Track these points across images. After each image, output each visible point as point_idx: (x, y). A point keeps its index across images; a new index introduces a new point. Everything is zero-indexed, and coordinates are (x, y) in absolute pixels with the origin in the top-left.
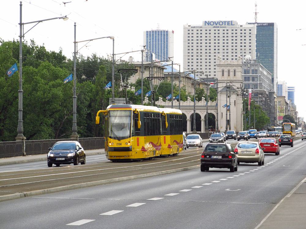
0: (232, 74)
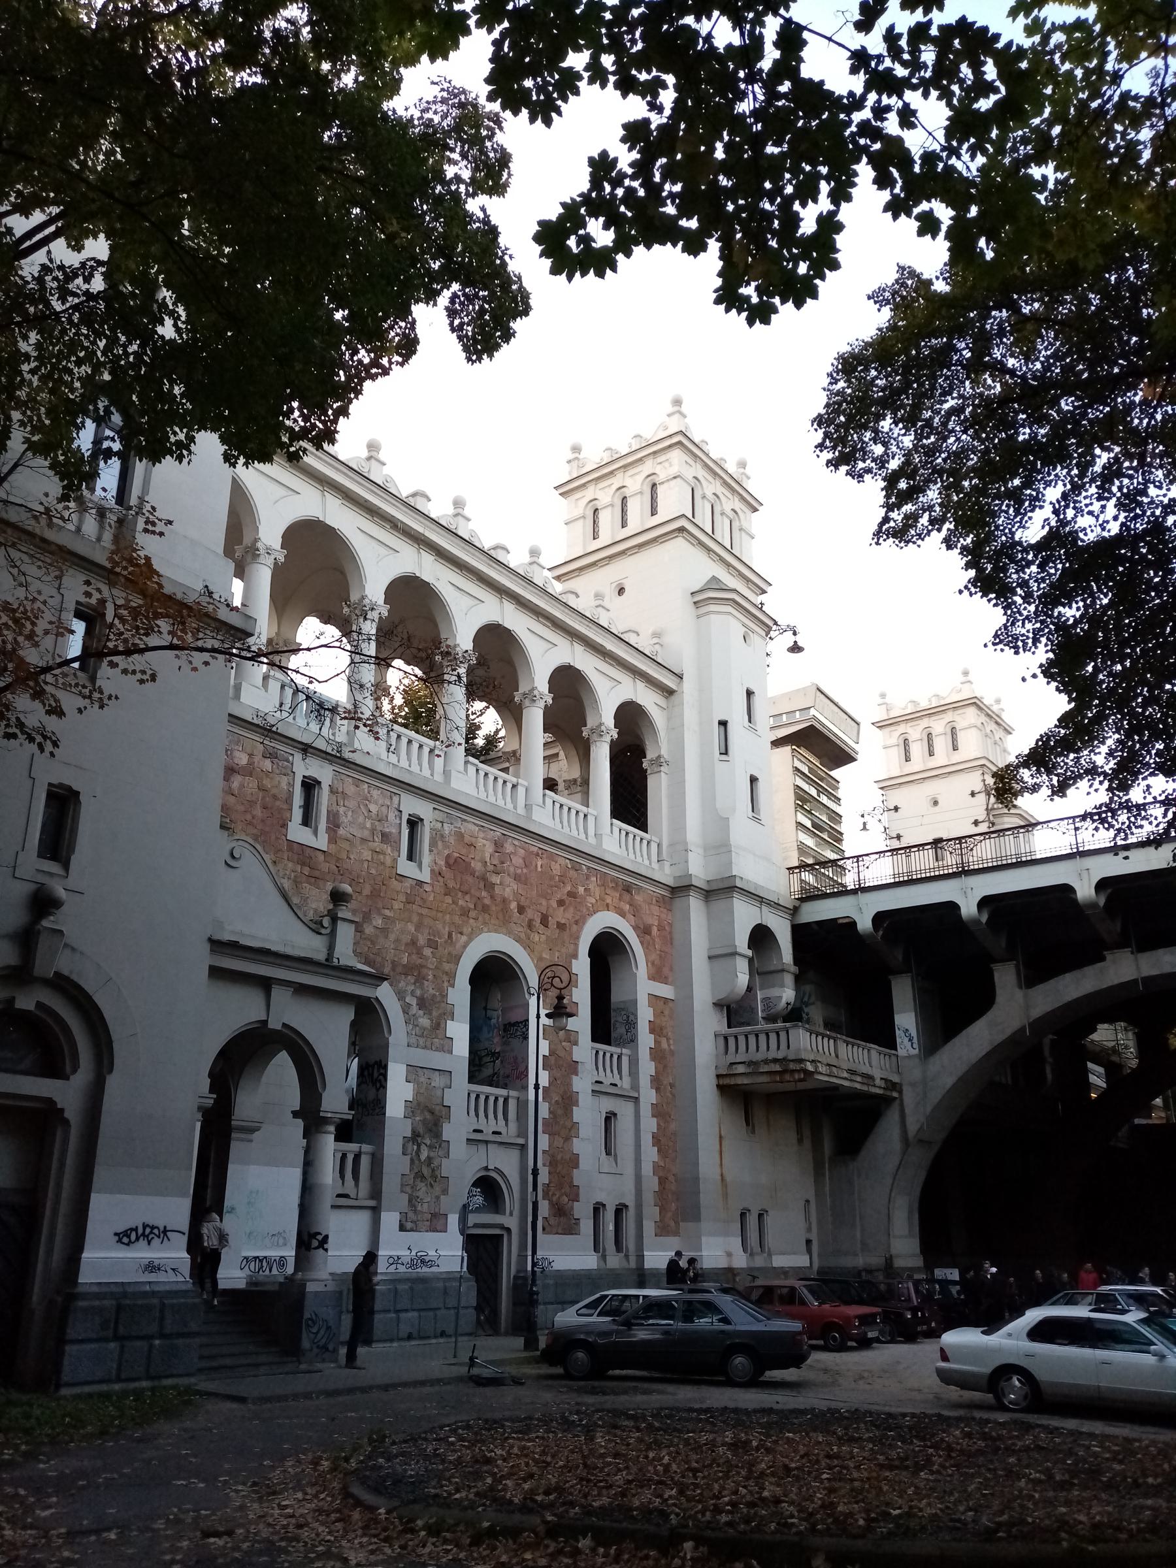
0: (941, 744)
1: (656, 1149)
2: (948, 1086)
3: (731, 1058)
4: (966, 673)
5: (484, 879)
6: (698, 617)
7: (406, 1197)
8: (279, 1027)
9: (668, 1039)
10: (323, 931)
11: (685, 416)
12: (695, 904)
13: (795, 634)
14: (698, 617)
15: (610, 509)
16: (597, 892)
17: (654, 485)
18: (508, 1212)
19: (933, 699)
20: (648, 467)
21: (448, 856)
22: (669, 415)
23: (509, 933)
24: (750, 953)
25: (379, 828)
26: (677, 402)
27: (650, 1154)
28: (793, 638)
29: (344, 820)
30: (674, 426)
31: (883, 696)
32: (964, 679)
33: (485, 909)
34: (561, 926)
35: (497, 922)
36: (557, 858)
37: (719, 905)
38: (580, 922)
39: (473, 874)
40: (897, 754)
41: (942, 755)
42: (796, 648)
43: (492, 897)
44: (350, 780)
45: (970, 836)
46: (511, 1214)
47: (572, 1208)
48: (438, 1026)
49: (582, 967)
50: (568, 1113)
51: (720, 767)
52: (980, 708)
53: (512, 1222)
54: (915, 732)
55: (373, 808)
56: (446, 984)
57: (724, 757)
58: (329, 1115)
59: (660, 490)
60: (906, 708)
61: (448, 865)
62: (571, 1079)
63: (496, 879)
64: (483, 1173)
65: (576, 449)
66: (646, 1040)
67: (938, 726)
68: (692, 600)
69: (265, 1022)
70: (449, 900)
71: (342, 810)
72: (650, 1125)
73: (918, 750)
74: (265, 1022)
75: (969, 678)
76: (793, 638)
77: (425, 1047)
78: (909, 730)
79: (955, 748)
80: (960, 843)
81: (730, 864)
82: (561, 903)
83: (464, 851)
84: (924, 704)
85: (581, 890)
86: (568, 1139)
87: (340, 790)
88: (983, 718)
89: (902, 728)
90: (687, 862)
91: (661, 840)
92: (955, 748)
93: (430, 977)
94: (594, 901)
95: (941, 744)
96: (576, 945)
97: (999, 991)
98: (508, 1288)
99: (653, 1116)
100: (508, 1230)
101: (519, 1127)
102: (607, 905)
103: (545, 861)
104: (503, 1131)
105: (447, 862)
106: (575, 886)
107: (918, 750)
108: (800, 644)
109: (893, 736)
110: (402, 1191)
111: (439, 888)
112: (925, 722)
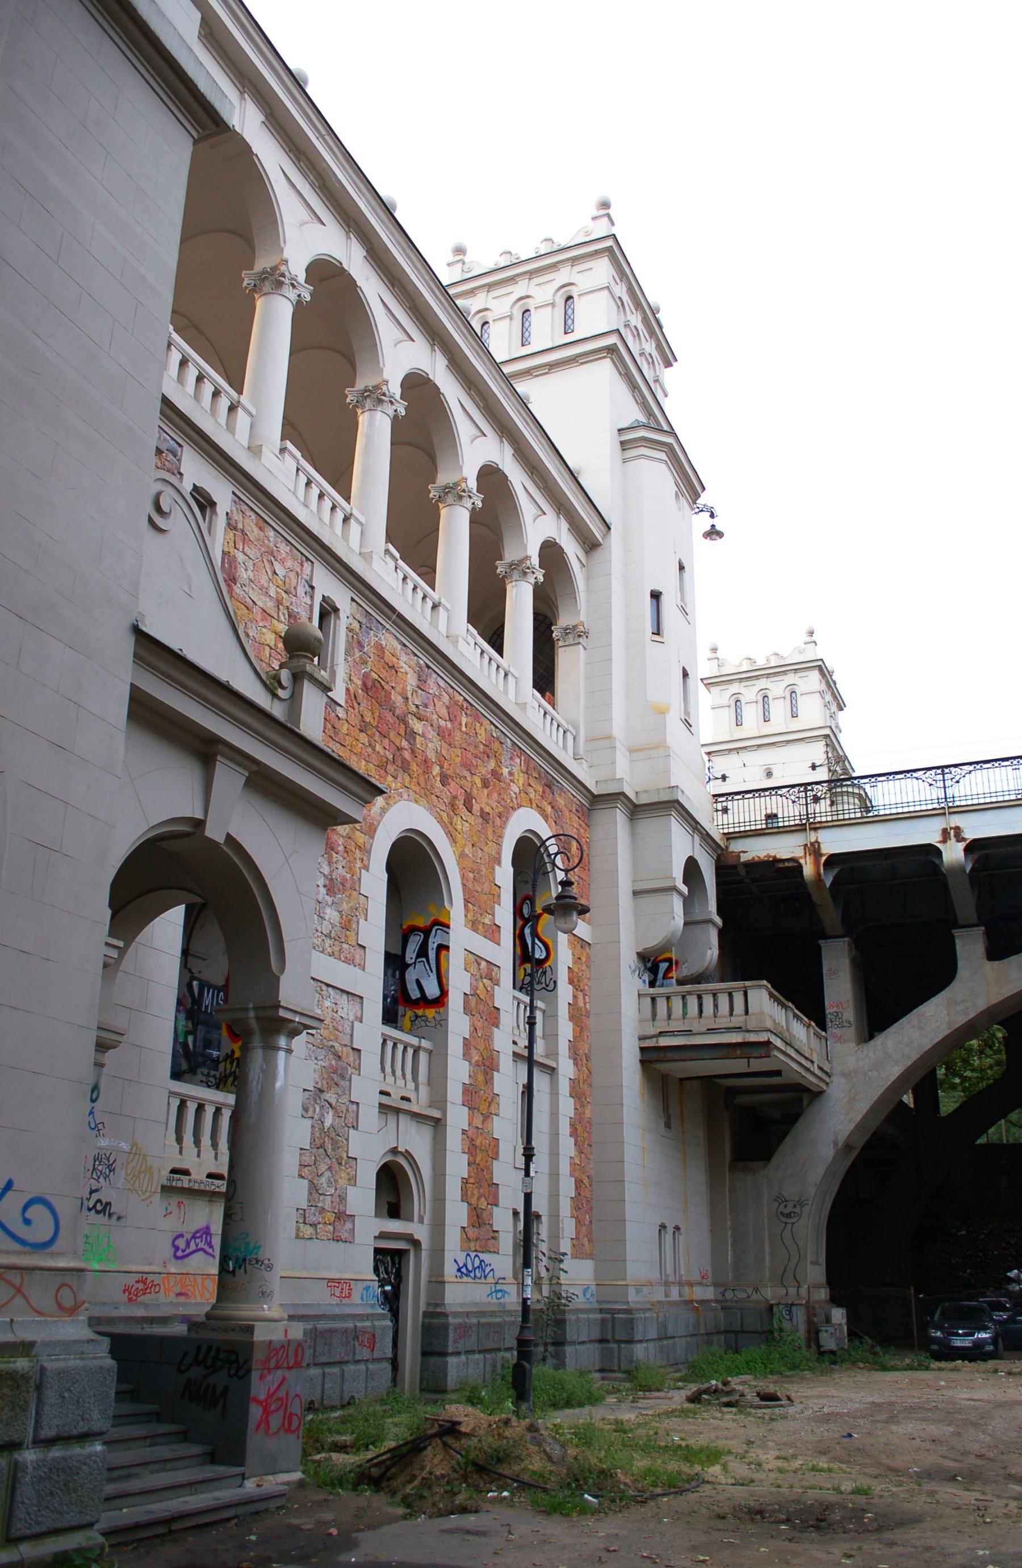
0: (779, 710)
1: (572, 1140)
2: (893, 1078)
3: (662, 1026)
4: (811, 633)
5: (403, 720)
6: (625, 461)
7: (305, 1183)
8: (220, 839)
9: (585, 995)
10: (281, 693)
11: (613, 224)
12: (620, 817)
13: (712, 516)
14: (625, 461)
15: (508, 320)
16: (521, 779)
17: (570, 298)
18: (416, 1218)
19: (772, 658)
20: (564, 275)
21: (366, 676)
22: (594, 219)
23: (431, 808)
24: (685, 889)
25: (286, 603)
26: (605, 205)
27: (567, 1146)
28: (710, 522)
29: (243, 575)
30: (601, 229)
31: (714, 650)
32: (809, 639)
33: (405, 767)
34: (484, 816)
35: (417, 789)
36: (483, 719)
37: (648, 825)
38: (504, 816)
39: (392, 710)
40: (728, 715)
41: (780, 720)
42: (713, 533)
43: (413, 751)
44: (254, 516)
45: (956, 766)
46: (421, 1220)
47: (491, 1214)
48: (348, 924)
49: (505, 875)
50: (489, 1081)
51: (653, 650)
52: (823, 675)
53: (420, 1231)
54: (749, 693)
55: (280, 571)
56: (359, 864)
57: (656, 638)
58: (288, 1015)
59: (578, 304)
60: (741, 665)
61: (365, 687)
62: (492, 1033)
63: (418, 726)
64: (389, 1158)
65: (460, 250)
66: (565, 992)
67: (777, 688)
68: (617, 440)
69: (199, 824)
70: (363, 738)
71: (240, 557)
72: (567, 1107)
73: (751, 714)
74: (199, 824)
75: (815, 637)
76: (710, 522)
77: (332, 955)
78: (742, 690)
79: (794, 715)
80: (943, 774)
81: (667, 772)
82: (485, 784)
83: (384, 674)
84: (761, 662)
85: (505, 771)
86: (487, 1117)
87: (240, 526)
88: (824, 687)
89: (735, 688)
90: (614, 763)
91: (577, 731)
92: (794, 715)
93: (341, 848)
94: (517, 790)
95: (779, 710)
96: (499, 845)
97: (960, 964)
98: (413, 1334)
99: (571, 1096)
100: (416, 1243)
101: (432, 1094)
102: (530, 800)
103: (470, 719)
104: (412, 1096)
105: (364, 684)
106: (499, 763)
107: (751, 714)
108: (718, 528)
109: (724, 695)
110: (301, 1176)
111: (355, 720)
112: (762, 683)
